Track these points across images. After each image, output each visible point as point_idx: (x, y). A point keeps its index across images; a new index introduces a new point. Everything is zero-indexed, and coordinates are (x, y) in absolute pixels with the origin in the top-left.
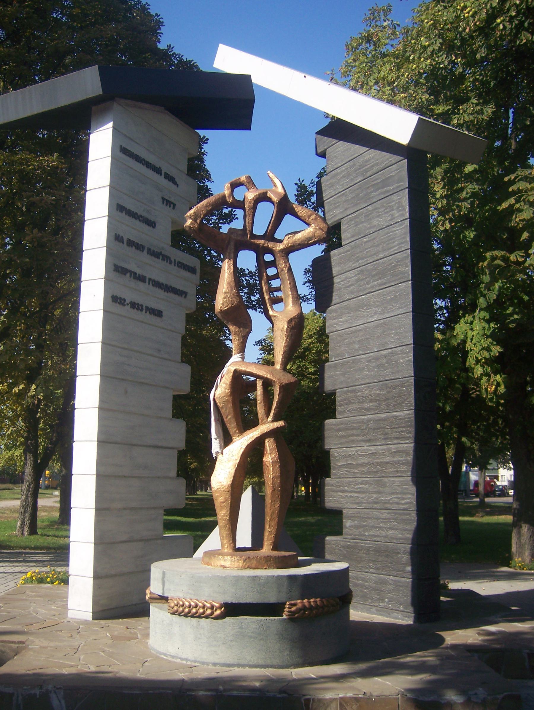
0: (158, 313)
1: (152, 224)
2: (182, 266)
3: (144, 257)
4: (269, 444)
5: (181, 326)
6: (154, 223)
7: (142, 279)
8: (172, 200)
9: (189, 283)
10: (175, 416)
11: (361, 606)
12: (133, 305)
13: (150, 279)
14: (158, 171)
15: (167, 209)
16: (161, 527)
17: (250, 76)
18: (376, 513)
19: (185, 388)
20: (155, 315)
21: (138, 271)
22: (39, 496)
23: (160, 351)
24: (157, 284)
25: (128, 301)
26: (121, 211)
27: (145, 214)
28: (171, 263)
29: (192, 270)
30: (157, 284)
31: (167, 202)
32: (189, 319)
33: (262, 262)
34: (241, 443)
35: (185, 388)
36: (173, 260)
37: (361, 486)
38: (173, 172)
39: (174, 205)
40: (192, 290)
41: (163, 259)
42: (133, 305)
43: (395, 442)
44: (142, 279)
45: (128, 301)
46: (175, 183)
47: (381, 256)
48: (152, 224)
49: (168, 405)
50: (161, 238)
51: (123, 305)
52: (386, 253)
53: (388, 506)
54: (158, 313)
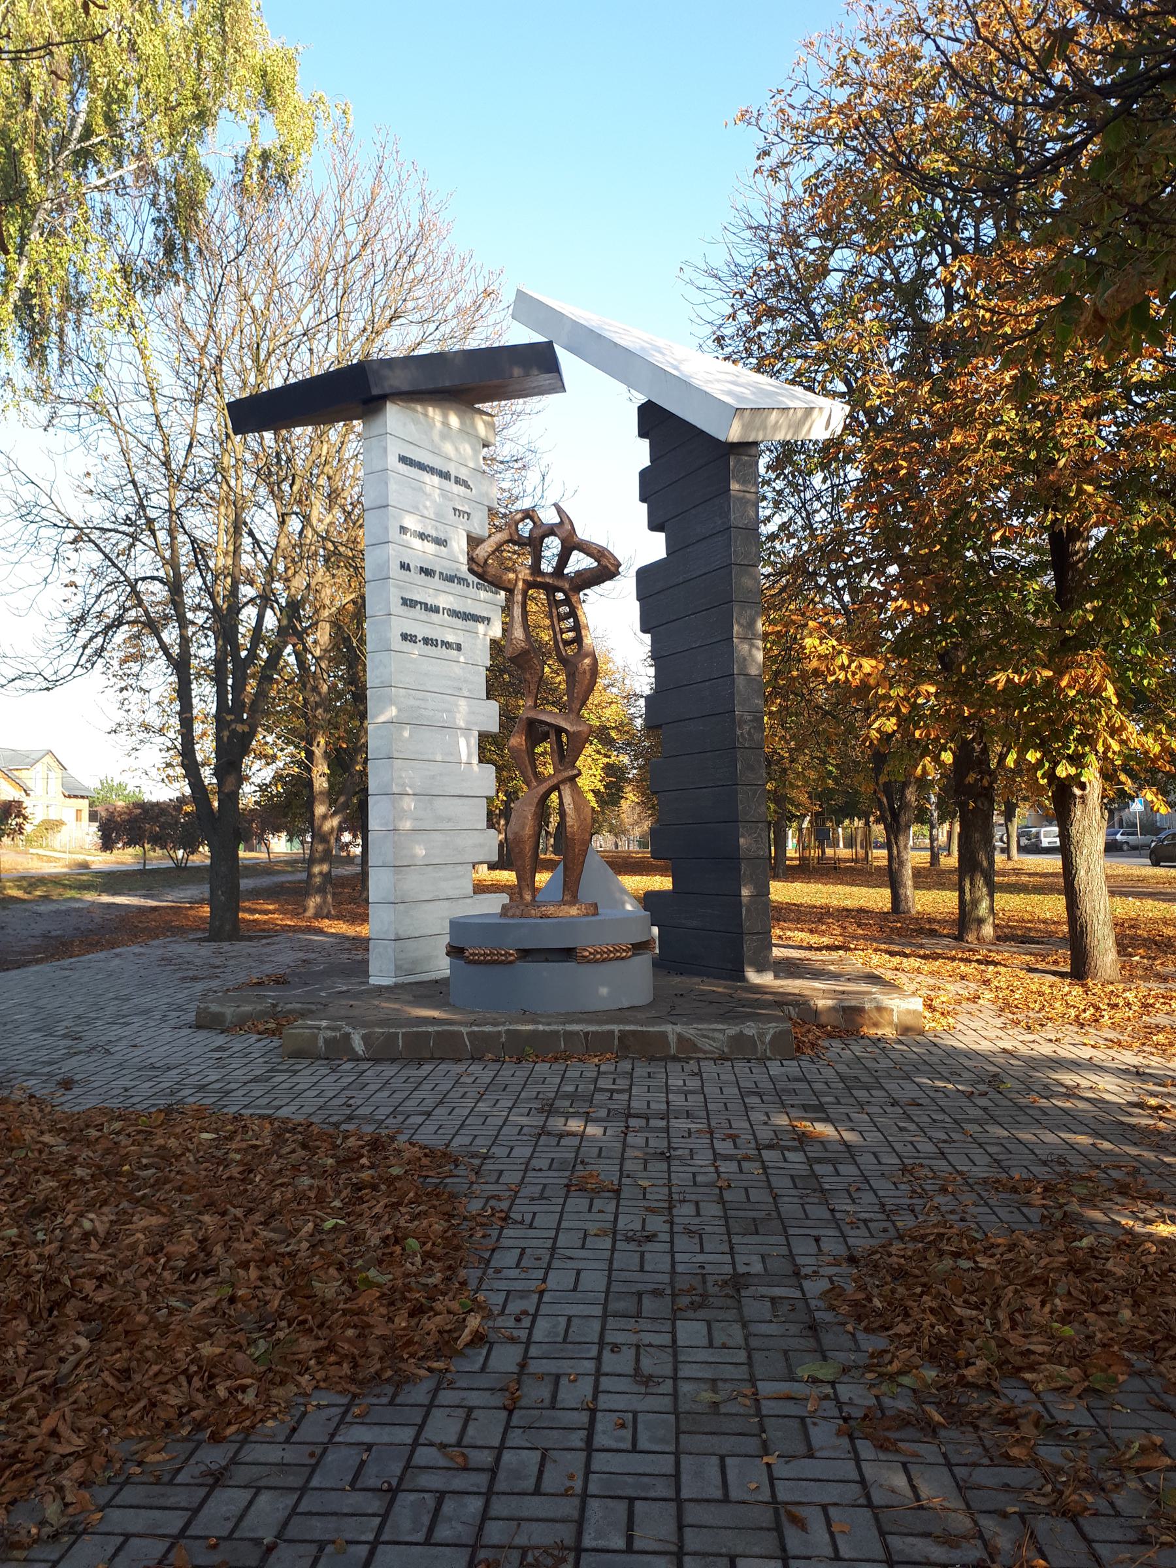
3: (436, 582)
12: (426, 641)
35: (494, 728)
46: (468, 487)
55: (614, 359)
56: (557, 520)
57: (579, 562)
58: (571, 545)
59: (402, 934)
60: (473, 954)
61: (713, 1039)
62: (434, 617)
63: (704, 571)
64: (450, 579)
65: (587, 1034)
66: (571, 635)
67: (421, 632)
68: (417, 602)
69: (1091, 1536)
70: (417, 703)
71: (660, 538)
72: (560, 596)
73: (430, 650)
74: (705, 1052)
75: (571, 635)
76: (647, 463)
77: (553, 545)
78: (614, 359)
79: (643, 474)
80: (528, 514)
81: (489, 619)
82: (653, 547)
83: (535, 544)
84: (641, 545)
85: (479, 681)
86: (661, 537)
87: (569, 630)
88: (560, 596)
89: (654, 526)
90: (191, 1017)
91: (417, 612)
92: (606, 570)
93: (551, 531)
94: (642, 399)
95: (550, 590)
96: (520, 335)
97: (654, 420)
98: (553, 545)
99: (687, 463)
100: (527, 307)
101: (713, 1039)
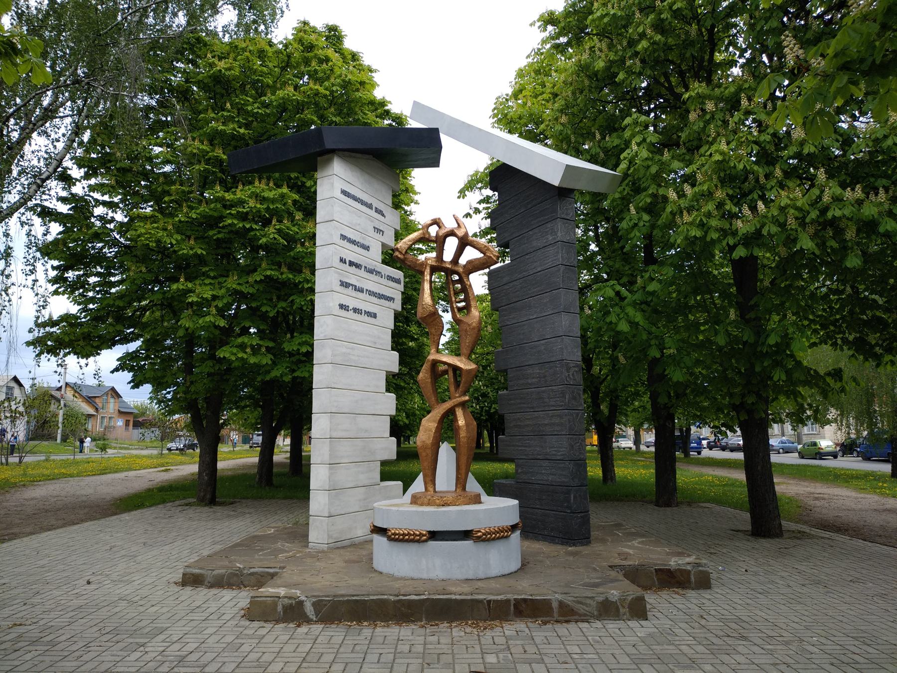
1: (367, 248)
2: (390, 278)
3: (362, 273)
4: (459, 413)
5: (391, 324)
7: (361, 290)
9: (484, 647)
10: (388, 390)
12: (355, 310)
14: (370, 206)
17: (438, 166)
19: (395, 369)
22: (743, 493)
24: (372, 293)
25: (351, 308)
27: (362, 241)
29: (398, 281)
30: (372, 293)
32: (397, 316)
34: (438, 411)
35: (395, 369)
38: (381, 207)
40: (398, 298)
42: (355, 310)
44: (361, 290)
45: (351, 308)
46: (383, 215)
47: (539, 269)
48: (367, 248)
49: (383, 384)
52: (543, 268)
53: (548, 457)
59: (333, 512)
60: (395, 534)
61: (586, 604)
62: (359, 295)
64: (371, 271)
65: (489, 602)
66: (463, 304)
73: (356, 316)
74: (580, 615)
75: (463, 304)
77: (451, 245)
80: (436, 222)
81: (393, 299)
83: (440, 241)
90: (178, 577)
91: (350, 291)
93: (452, 233)
98: (451, 245)
101: (586, 604)
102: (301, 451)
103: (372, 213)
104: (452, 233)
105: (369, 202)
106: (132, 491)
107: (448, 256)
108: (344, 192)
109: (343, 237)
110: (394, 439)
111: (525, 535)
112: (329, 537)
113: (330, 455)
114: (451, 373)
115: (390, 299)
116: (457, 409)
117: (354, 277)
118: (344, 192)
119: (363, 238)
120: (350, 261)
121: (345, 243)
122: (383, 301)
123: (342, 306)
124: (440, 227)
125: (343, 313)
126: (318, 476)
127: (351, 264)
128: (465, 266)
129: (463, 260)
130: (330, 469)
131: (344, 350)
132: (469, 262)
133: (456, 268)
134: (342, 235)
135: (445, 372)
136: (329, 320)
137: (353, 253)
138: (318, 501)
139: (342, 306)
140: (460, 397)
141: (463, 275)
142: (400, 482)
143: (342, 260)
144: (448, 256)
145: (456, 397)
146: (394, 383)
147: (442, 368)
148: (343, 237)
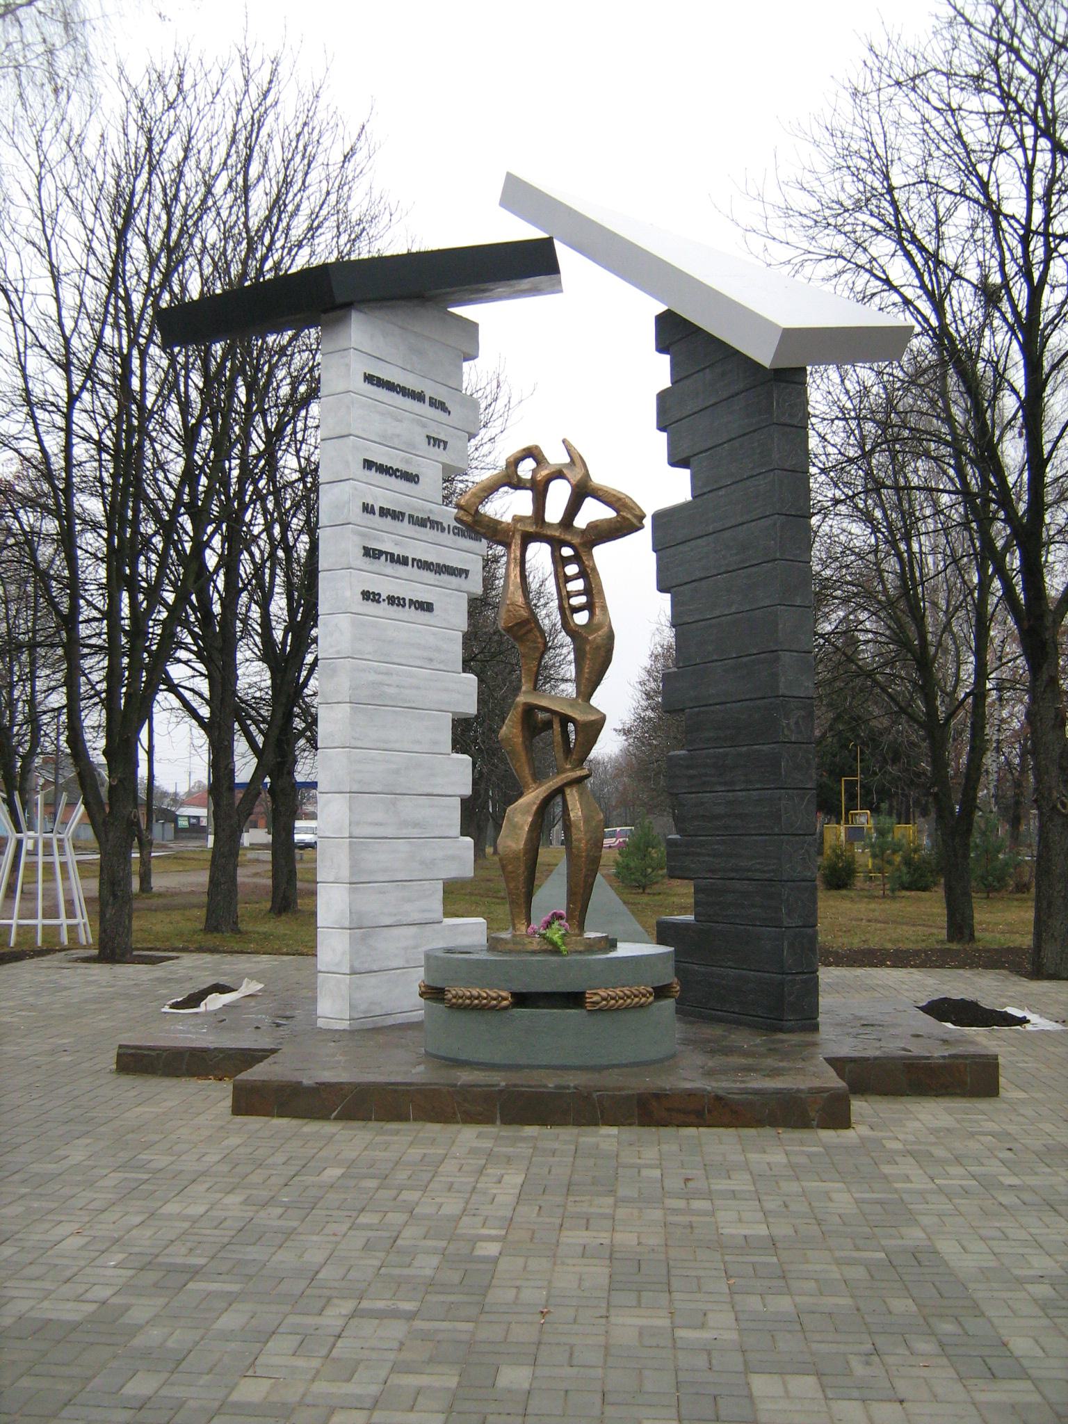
0: (427, 607)
1: (412, 478)
3: (405, 527)
6: (417, 476)
7: (403, 561)
8: (442, 437)
11: (1016, 903)
12: (392, 600)
13: (414, 560)
14: (419, 397)
15: (436, 451)
16: (436, 903)
17: (561, 291)
18: (737, 885)
19: (470, 707)
20: (423, 609)
21: (396, 551)
23: (431, 660)
24: (425, 565)
25: (384, 596)
26: (370, 468)
28: (443, 530)
30: (425, 565)
31: (435, 441)
33: (564, 593)
35: (470, 707)
36: (445, 525)
37: (707, 859)
39: (445, 443)
41: (432, 527)
42: (392, 600)
43: (758, 786)
44: (403, 561)
45: (384, 596)
48: (412, 478)
49: (447, 737)
50: (426, 496)
51: (378, 602)
54: (427, 607)
55: (626, 260)
56: (567, 460)
57: (592, 512)
58: (583, 491)
62: (401, 570)
63: (740, 520)
64: (422, 523)
66: (583, 599)
67: (386, 588)
68: (381, 553)
69: (53, 301)
70: (380, 678)
71: (684, 476)
72: (567, 552)
73: (394, 611)
76: (666, 383)
77: (559, 495)
78: (626, 260)
79: (663, 397)
80: (531, 453)
81: (466, 572)
82: (671, 488)
83: (539, 491)
84: (665, 487)
85: (456, 651)
86: (685, 474)
87: (579, 594)
88: (567, 552)
89: (677, 461)
91: (382, 565)
92: (624, 523)
94: (662, 308)
95: (556, 544)
96: (521, 231)
97: (674, 332)
98: (559, 495)
99: (726, 389)
100: (518, 195)
102: (292, 873)
103: (424, 409)
104: (559, 474)
105: (418, 390)
106: (967, 973)
107: (554, 513)
108: (369, 378)
109: (368, 464)
110: (469, 840)
111: (686, 1010)
112: (352, 1007)
113: (351, 867)
114: (557, 727)
115: (462, 573)
116: (568, 791)
117: (391, 538)
118: (369, 378)
119: (407, 462)
120: (381, 509)
121: (373, 475)
122: (445, 578)
123: (366, 595)
124: (538, 463)
125: (370, 607)
126: (331, 903)
127: (384, 512)
128: (583, 532)
129: (581, 522)
130: (352, 891)
131: (372, 677)
132: (593, 526)
133: (568, 538)
134: (366, 461)
135: (548, 725)
136: (344, 621)
137: (386, 492)
138: (333, 947)
139: (366, 595)
140: (572, 770)
141: (581, 549)
142: (481, 920)
143: (367, 509)
144: (554, 513)
145: (565, 771)
146: (464, 735)
147: (541, 716)
148: (368, 464)
